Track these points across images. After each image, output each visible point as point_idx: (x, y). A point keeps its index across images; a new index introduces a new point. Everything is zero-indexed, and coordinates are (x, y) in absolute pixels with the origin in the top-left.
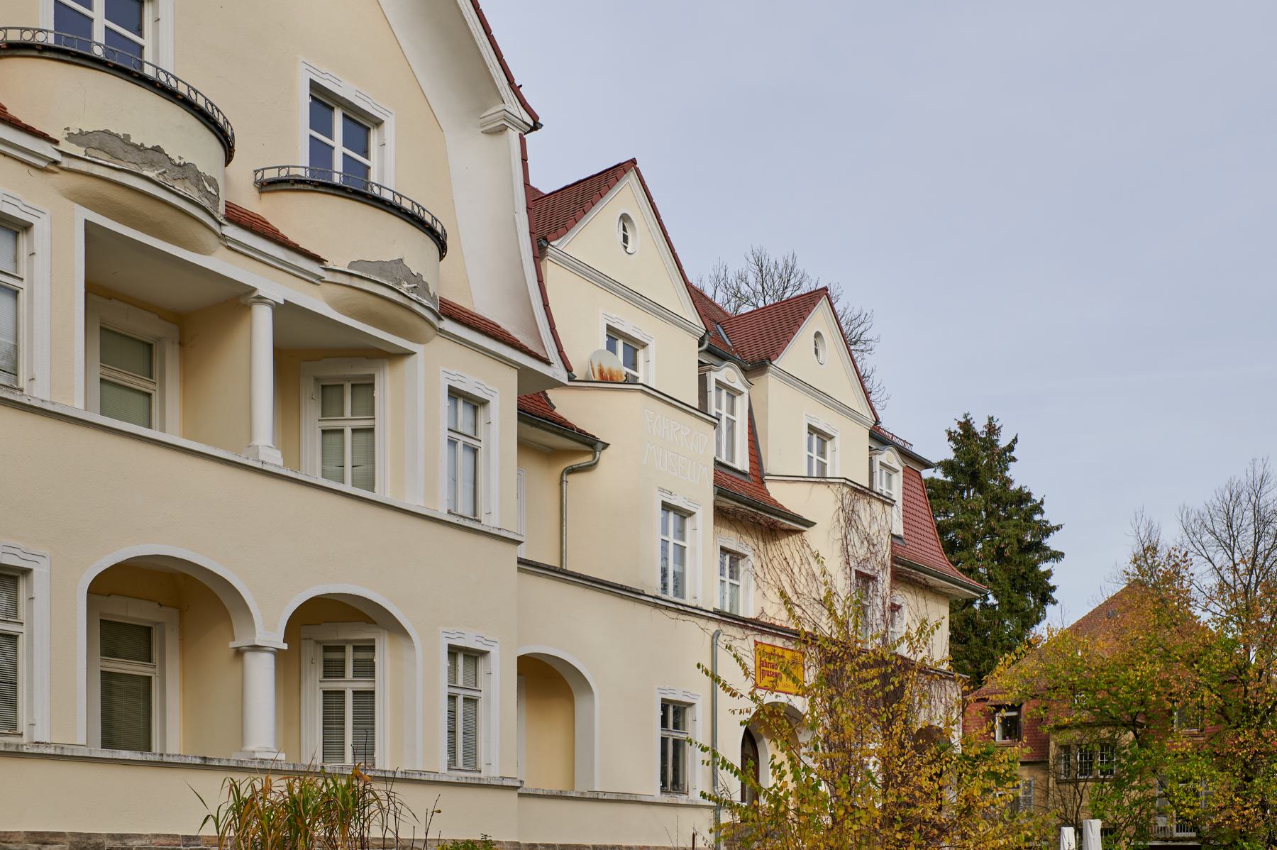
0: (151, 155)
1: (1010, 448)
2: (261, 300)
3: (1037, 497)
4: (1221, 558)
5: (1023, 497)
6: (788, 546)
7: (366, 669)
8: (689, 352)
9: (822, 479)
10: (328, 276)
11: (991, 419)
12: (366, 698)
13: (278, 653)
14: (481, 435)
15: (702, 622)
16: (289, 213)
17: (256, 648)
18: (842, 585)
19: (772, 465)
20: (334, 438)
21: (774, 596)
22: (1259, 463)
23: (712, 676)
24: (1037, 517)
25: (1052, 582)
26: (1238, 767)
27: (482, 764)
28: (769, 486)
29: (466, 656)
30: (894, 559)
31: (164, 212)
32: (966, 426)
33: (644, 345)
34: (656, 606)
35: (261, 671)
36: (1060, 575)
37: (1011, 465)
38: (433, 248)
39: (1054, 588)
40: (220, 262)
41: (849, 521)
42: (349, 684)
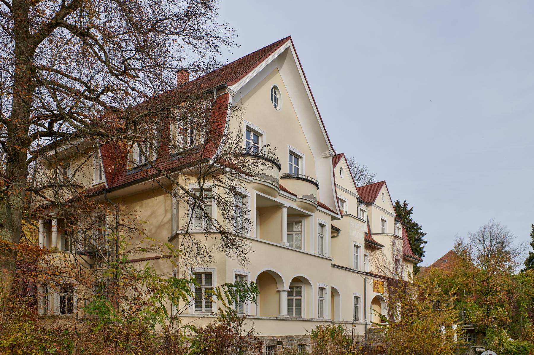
0: (270, 177)
1: (411, 210)
2: (285, 207)
3: (419, 225)
4: (481, 247)
5: (415, 225)
6: (378, 252)
7: (300, 293)
8: (355, 201)
9: (383, 234)
10: (298, 200)
11: (405, 201)
12: (299, 301)
13: (288, 292)
14: (324, 233)
15: (362, 275)
16: (287, 184)
17: (284, 291)
18: (392, 262)
19: (373, 231)
20: (291, 236)
21: (374, 266)
22: (492, 220)
23: (221, 233)
24: (419, 231)
25: (423, 250)
26: (486, 307)
27: (324, 316)
28: (373, 236)
29: (322, 289)
30: (403, 255)
31: (270, 190)
32: (397, 203)
33: (345, 201)
34: (353, 272)
35: (284, 297)
36: (426, 248)
37: (411, 215)
38: (316, 188)
39: (424, 252)
40: (279, 199)
41: (393, 245)
42: (295, 297)
